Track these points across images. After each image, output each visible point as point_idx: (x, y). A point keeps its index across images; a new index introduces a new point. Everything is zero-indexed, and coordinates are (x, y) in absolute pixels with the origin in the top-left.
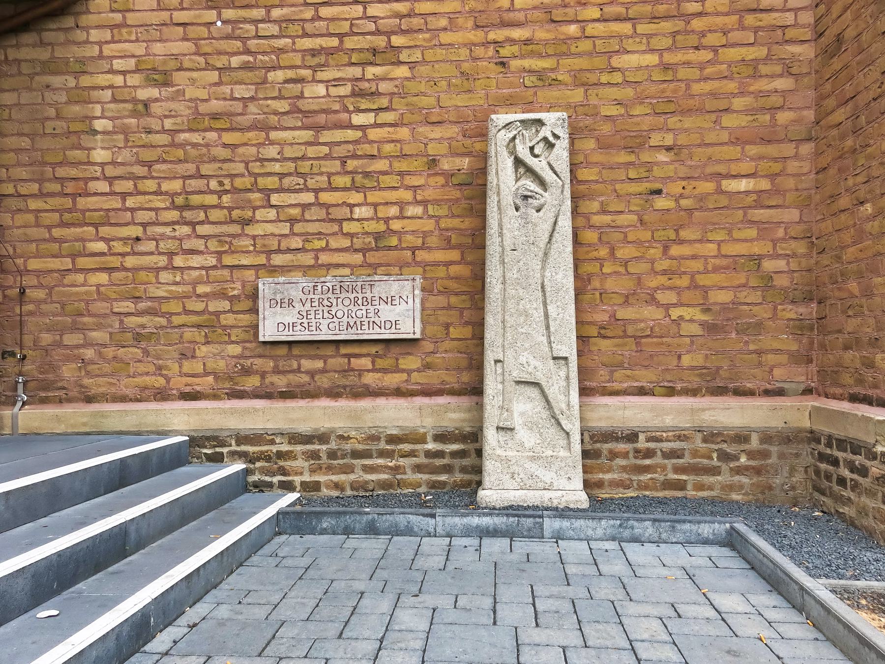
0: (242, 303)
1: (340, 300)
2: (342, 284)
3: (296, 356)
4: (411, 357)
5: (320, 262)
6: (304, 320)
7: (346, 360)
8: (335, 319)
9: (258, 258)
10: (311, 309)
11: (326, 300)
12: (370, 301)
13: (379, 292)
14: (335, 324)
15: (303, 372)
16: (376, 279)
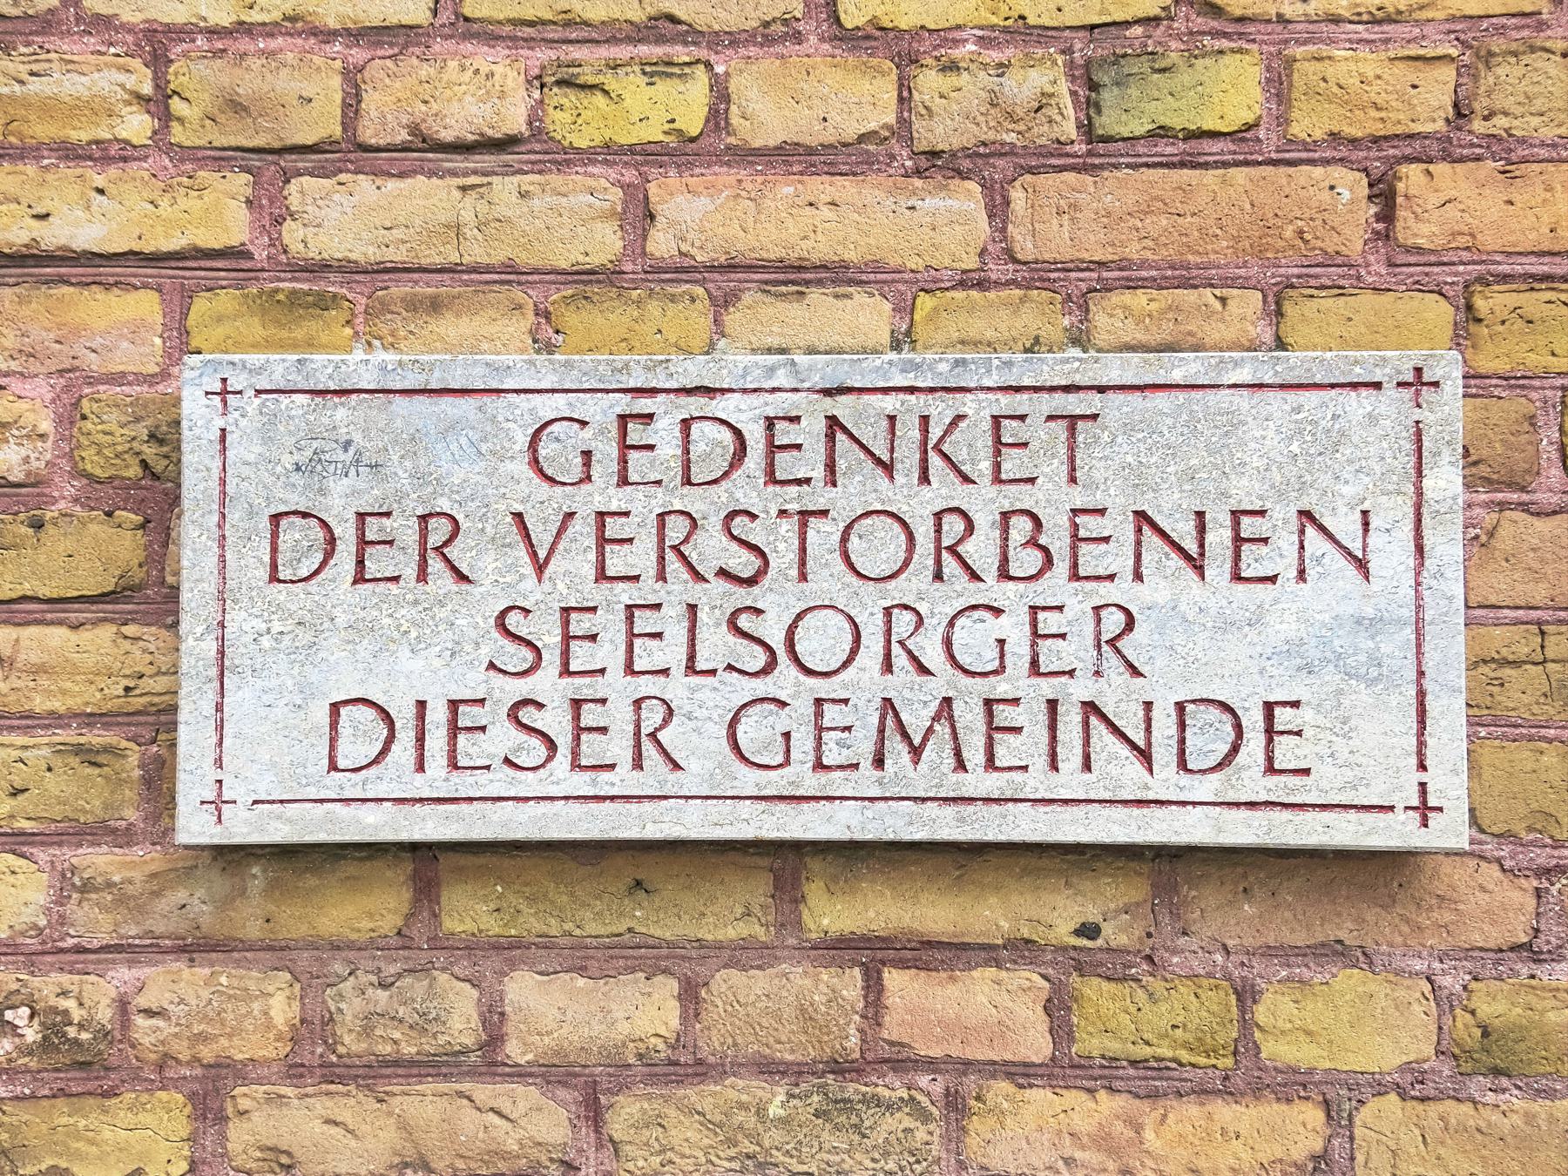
0: (57, 541)
1: (823, 535)
2: (842, 407)
3: (472, 947)
4: (1349, 980)
5: (661, 244)
6: (547, 684)
7: (851, 985)
8: (786, 679)
9: (192, 203)
10: (594, 593)
11: (714, 523)
12: (1058, 543)
13: (1137, 478)
14: (783, 720)
15: (520, 1074)
16: (1113, 376)
